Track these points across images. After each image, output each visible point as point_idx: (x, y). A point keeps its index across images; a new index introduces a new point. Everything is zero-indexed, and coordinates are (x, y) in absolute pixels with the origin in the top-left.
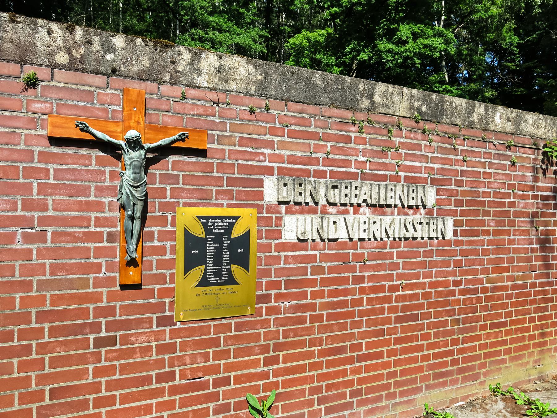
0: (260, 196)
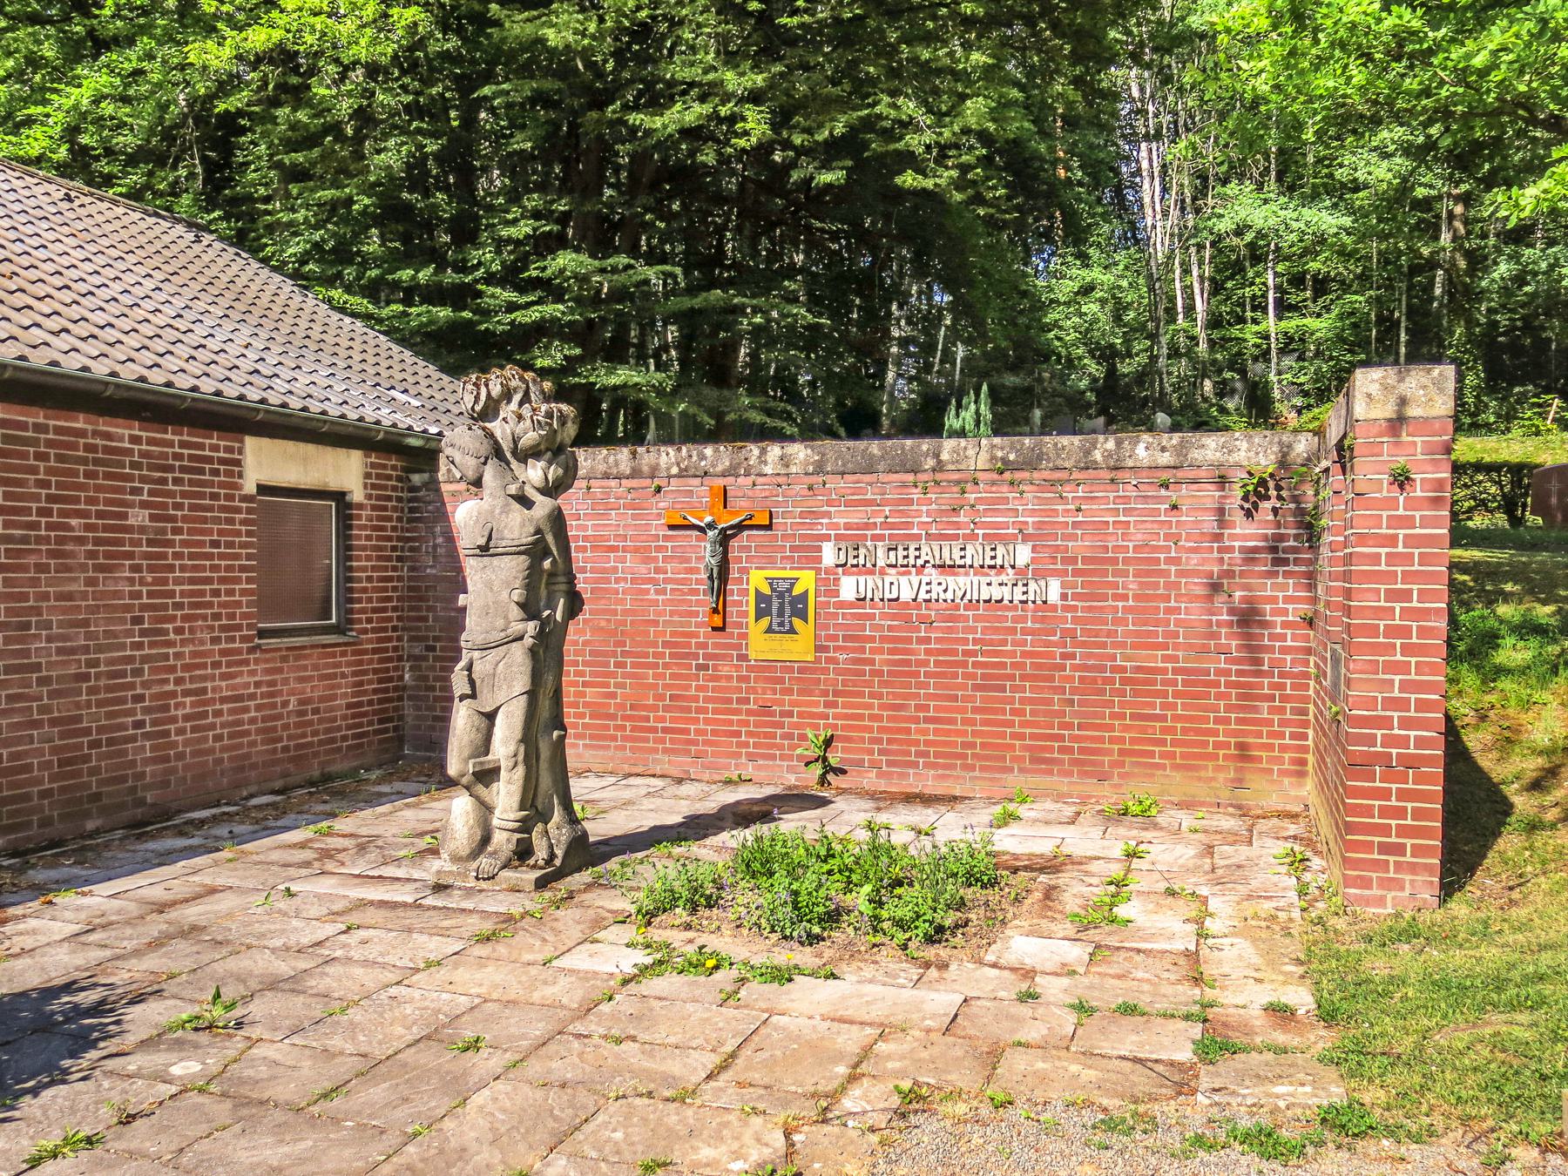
0: (819, 560)
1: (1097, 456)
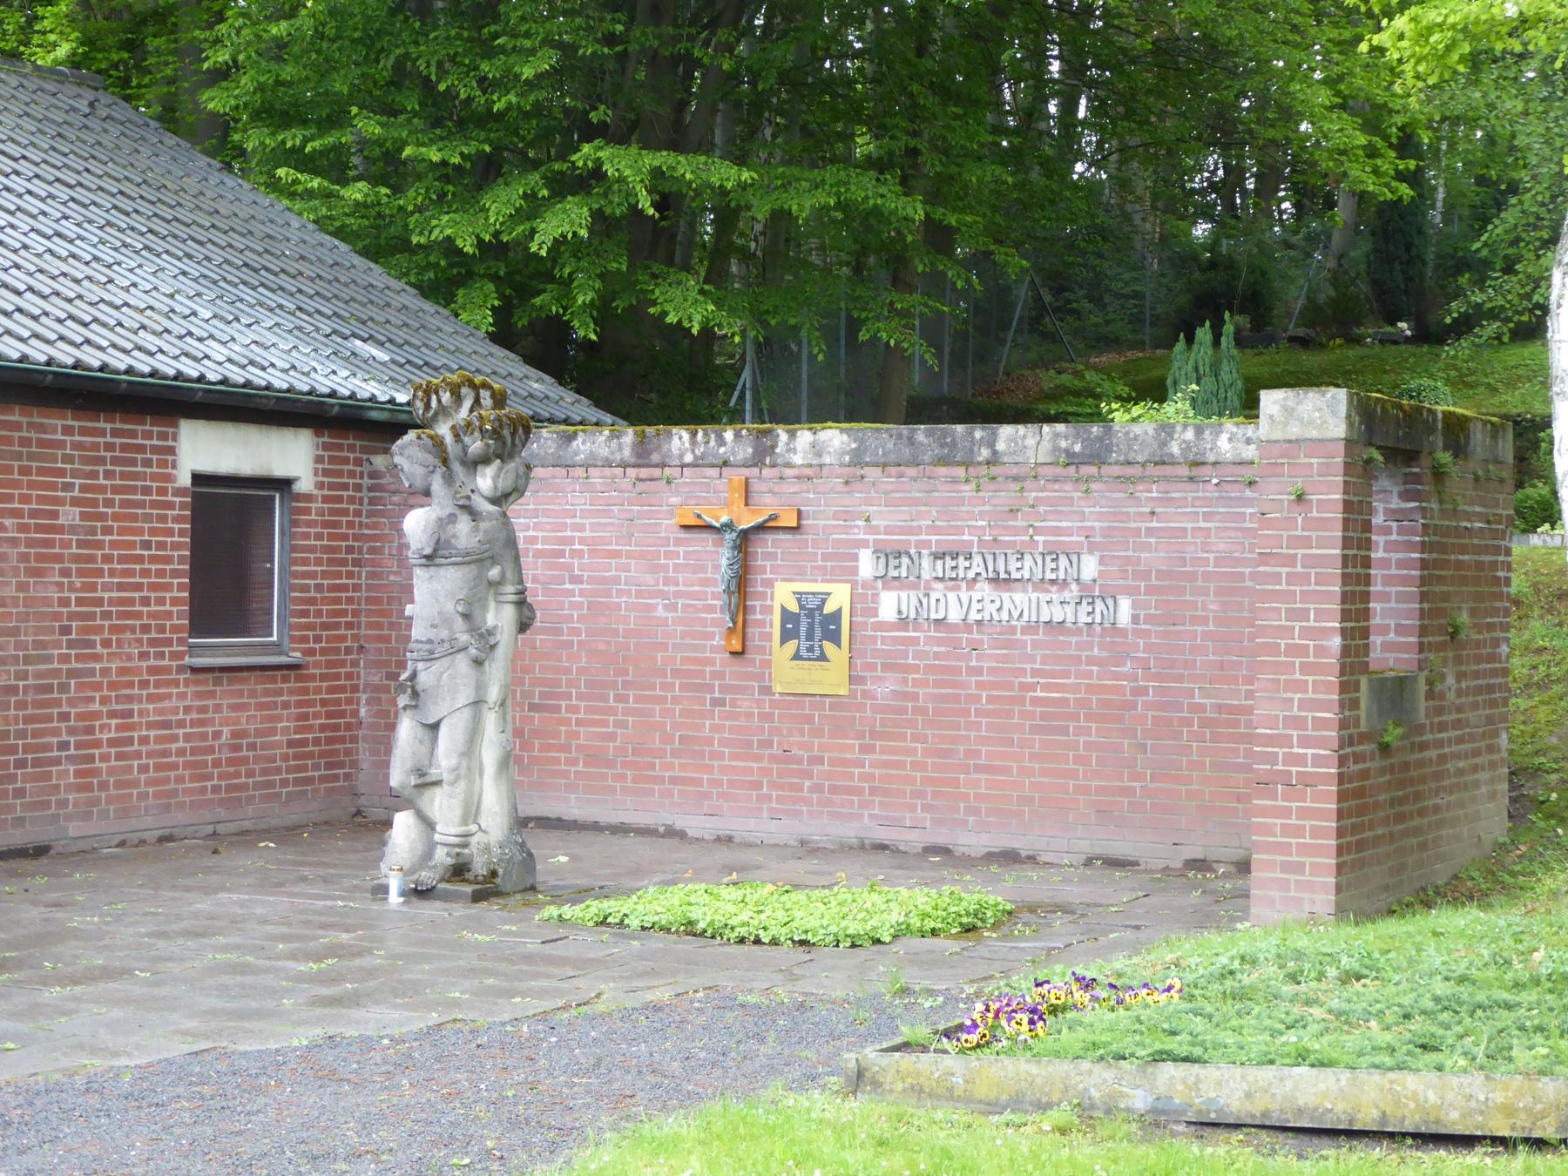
1: (1175, 448)
